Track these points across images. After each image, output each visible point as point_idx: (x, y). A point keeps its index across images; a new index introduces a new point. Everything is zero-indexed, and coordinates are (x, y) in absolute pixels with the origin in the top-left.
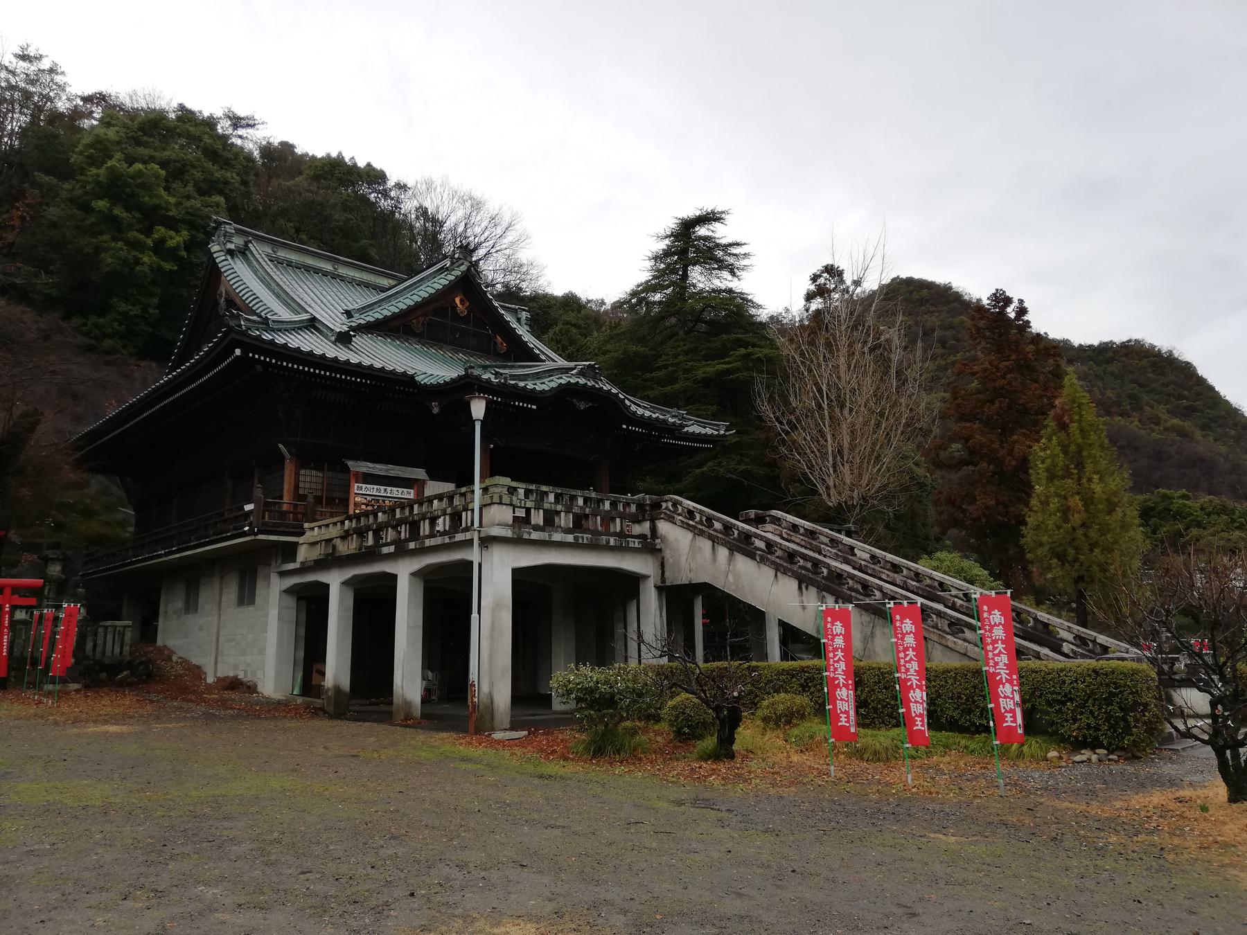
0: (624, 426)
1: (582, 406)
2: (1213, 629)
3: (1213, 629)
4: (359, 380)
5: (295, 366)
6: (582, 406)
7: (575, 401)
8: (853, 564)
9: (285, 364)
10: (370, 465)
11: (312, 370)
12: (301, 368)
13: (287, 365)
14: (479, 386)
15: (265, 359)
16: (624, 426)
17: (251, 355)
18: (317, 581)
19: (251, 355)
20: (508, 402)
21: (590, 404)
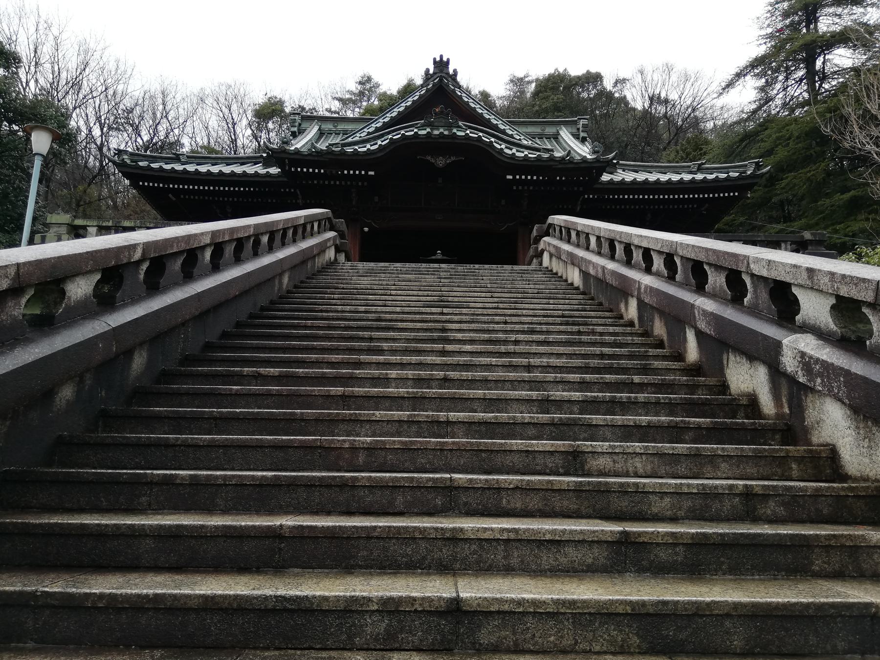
0: (510, 177)
1: (441, 162)
2: (666, 104)
3: (666, 104)
4: (232, 189)
5: (681, 196)
6: (441, 162)
7: (429, 158)
8: (478, 384)
9: (171, 186)
11: (666, 197)
12: (696, 196)
13: (174, 186)
14: (289, 159)
15: (154, 185)
16: (510, 177)
17: (141, 183)
18: (707, 276)
19: (141, 183)
20: (334, 172)
21: (453, 159)
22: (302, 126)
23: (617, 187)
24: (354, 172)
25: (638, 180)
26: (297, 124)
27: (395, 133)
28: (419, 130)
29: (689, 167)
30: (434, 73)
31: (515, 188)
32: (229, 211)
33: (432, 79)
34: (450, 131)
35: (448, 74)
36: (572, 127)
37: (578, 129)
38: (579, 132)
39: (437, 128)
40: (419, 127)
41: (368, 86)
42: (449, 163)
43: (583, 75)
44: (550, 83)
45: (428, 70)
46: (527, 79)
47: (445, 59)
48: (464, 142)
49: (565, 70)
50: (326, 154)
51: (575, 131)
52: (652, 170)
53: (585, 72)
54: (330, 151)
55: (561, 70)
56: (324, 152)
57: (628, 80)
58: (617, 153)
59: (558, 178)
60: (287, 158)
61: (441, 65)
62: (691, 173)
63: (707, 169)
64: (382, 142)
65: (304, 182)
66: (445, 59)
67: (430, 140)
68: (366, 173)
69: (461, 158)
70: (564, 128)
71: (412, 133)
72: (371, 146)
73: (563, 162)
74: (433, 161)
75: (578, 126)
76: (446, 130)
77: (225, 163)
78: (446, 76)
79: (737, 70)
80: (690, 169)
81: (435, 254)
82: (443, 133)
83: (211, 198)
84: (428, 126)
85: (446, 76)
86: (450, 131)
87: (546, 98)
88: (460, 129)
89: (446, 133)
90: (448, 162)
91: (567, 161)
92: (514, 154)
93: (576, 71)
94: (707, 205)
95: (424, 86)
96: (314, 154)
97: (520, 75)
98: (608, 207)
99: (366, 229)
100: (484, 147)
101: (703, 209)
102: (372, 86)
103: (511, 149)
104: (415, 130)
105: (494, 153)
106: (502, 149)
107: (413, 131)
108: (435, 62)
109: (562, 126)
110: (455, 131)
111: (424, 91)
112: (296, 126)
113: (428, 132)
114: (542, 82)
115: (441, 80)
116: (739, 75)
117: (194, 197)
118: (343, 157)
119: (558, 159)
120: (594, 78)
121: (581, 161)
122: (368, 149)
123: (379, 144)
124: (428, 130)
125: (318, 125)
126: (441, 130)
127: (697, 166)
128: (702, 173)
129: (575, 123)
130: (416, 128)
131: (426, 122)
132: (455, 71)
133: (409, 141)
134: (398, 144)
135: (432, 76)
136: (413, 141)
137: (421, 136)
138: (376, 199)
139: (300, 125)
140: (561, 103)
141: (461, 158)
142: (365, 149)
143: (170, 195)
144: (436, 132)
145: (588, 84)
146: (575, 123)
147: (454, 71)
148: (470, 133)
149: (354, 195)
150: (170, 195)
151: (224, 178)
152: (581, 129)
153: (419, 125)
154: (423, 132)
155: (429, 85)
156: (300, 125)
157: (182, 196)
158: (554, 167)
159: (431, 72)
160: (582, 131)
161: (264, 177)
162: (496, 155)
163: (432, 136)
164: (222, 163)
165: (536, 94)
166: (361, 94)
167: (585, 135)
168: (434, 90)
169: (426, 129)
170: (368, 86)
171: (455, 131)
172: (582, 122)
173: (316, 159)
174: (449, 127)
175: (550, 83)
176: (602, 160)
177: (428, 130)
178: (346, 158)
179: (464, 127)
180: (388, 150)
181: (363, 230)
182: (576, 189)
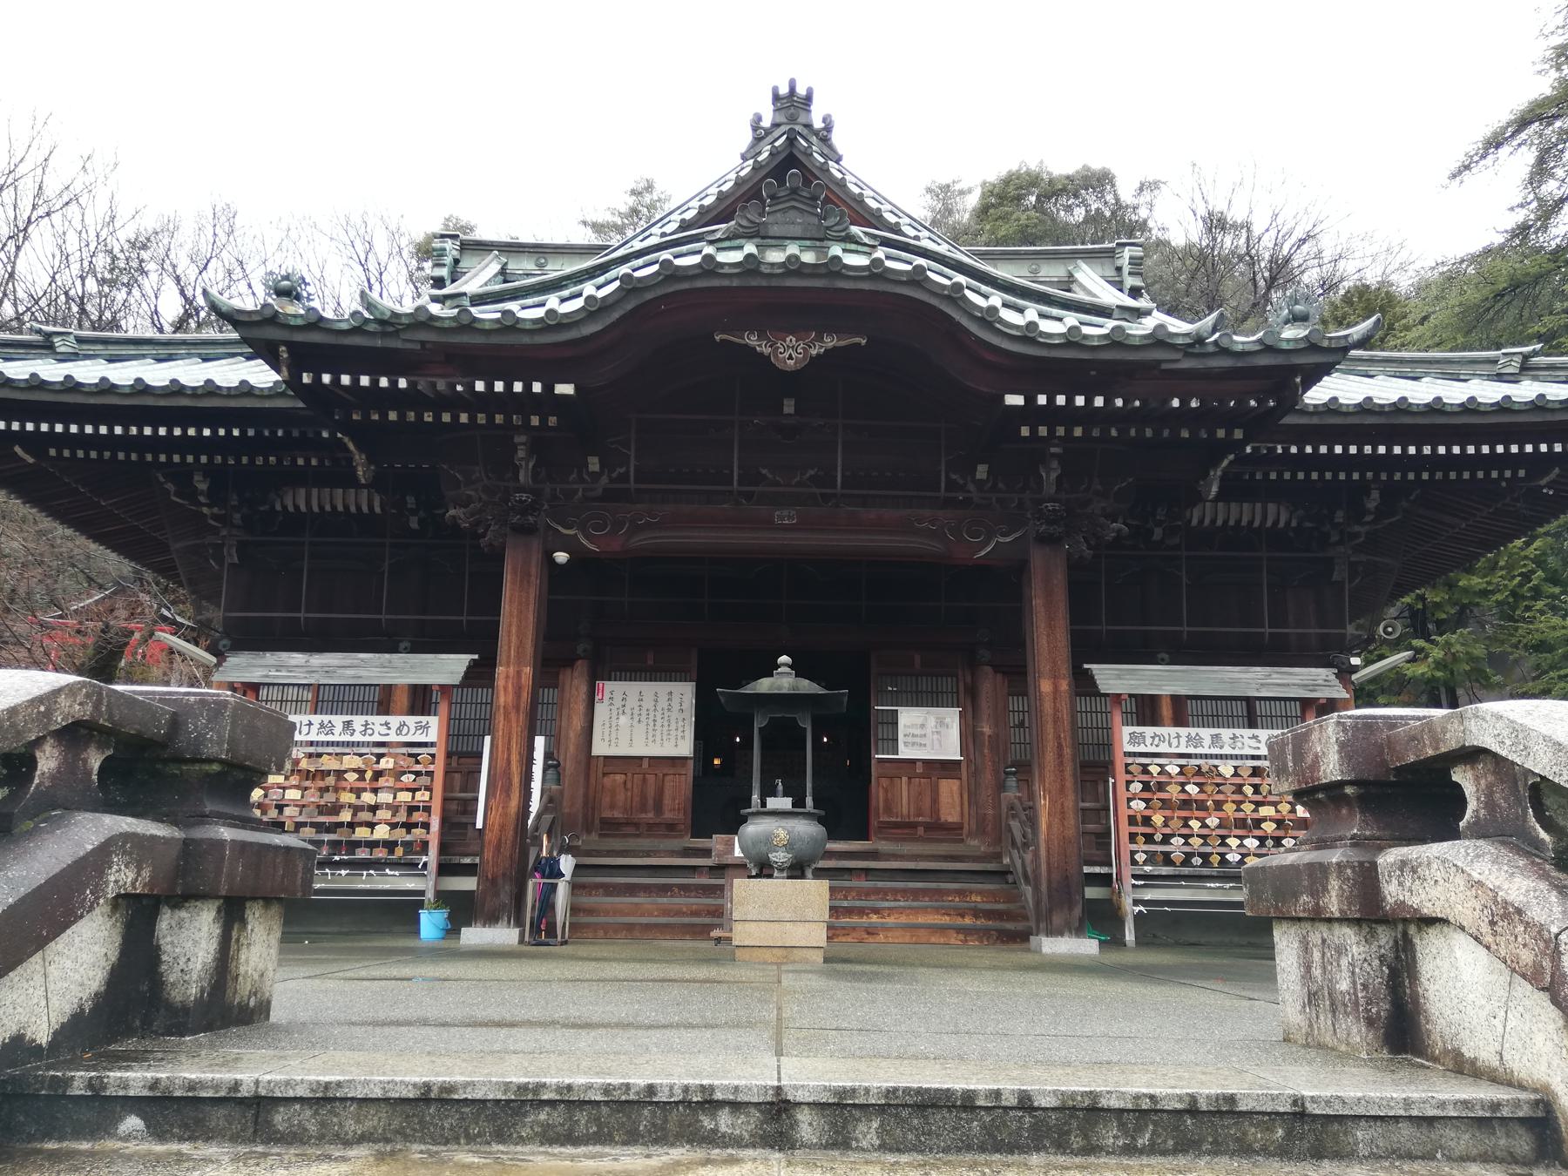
0: (1014, 400)
1: (790, 353)
6: (790, 353)
7: (752, 340)
10: (298, 658)
16: (1014, 400)
21: (830, 342)
22: (461, 265)
23: (1315, 420)
24: (509, 386)
25: (1376, 401)
26: (448, 260)
27: (640, 262)
28: (718, 249)
29: (1495, 362)
30: (776, 125)
31: (1025, 431)
32: (203, 486)
33: (770, 139)
34: (822, 250)
35: (808, 126)
36: (1102, 264)
37: (1119, 269)
38: (1120, 276)
39: (780, 241)
40: (719, 240)
41: (647, 199)
42: (818, 355)
43: (1077, 172)
44: (1012, 187)
45: (758, 118)
46: (957, 187)
47: (801, 91)
48: (866, 286)
49: (1041, 162)
50: (409, 327)
51: (1111, 272)
52: (1372, 369)
53: (1079, 167)
54: (465, 320)
55: (1033, 166)
56: (404, 320)
57: (1164, 183)
58: (1379, 320)
59: (1176, 403)
60: (286, 343)
61: (792, 103)
62: (1500, 378)
63: (1360, 360)
64: (599, 288)
65: (355, 417)
66: (801, 91)
67: (754, 282)
68: (548, 388)
69: (857, 340)
70: (1084, 266)
71: (696, 259)
72: (563, 300)
73: (1197, 349)
74: (767, 350)
75: (1118, 263)
76: (809, 248)
77: (199, 356)
78: (805, 132)
79: (1488, 131)
80: (1497, 369)
81: (769, 669)
82: (797, 258)
83: (236, 433)
84: (749, 237)
85: (805, 132)
86: (822, 250)
87: (1004, 218)
88: (853, 247)
89: (808, 257)
90: (814, 352)
91: (1211, 349)
92: (1032, 325)
93: (1062, 165)
94: (1557, 470)
95: (749, 156)
96: (371, 327)
97: (944, 180)
98: (1273, 476)
99: (561, 557)
100: (934, 302)
101: (1543, 482)
102: (656, 198)
103: (1021, 310)
104: (709, 250)
105: (965, 322)
106: (993, 310)
107: (700, 252)
108: (776, 97)
109: (1079, 261)
110: (836, 250)
111: (749, 169)
112: (444, 265)
113: (749, 256)
114: (994, 186)
115: (791, 141)
116: (1495, 142)
117: (87, 454)
118: (465, 339)
119: (1180, 341)
120: (1099, 181)
121: (1257, 348)
122: (551, 312)
123: (585, 295)
124: (750, 248)
125: (499, 263)
126: (793, 249)
127: (1518, 359)
128: (1535, 378)
129: (1110, 254)
130: (711, 242)
131: (744, 223)
132: (827, 120)
133: (685, 286)
134: (649, 296)
135: (768, 132)
136: (700, 284)
137: (726, 270)
138: (594, 464)
139: (456, 261)
140: (1036, 225)
141: (857, 340)
142: (539, 313)
143: (17, 449)
144: (775, 256)
145: (1087, 189)
146: (1110, 254)
147: (824, 120)
148: (888, 257)
149: (521, 454)
150: (17, 449)
151: (149, 401)
152: (1126, 269)
153: (718, 235)
154: (735, 257)
155: (760, 153)
156: (456, 261)
157: (53, 452)
158: (1164, 366)
159: (766, 123)
160: (1130, 273)
161: (269, 397)
162: (973, 328)
163: (764, 269)
164: (189, 356)
165: (983, 211)
166: (634, 212)
167: (1138, 282)
168: (772, 166)
169: (741, 248)
170: (647, 199)
171: (836, 250)
172: (1127, 253)
173: (379, 343)
174: (819, 239)
175: (1012, 187)
176: (1240, 348)
177: (750, 248)
178: (479, 340)
179: (866, 240)
180: (616, 315)
181: (553, 560)
182: (1221, 433)
